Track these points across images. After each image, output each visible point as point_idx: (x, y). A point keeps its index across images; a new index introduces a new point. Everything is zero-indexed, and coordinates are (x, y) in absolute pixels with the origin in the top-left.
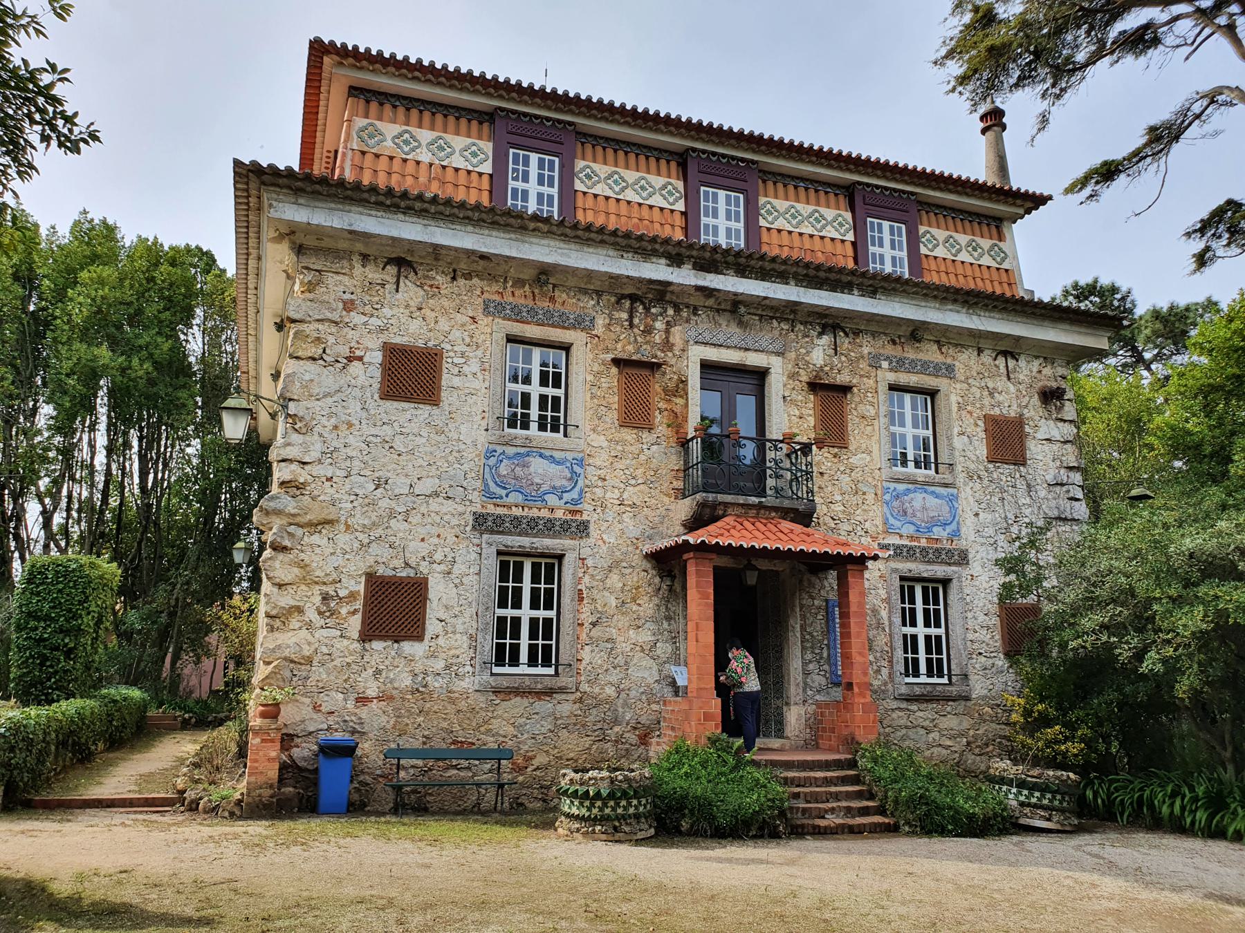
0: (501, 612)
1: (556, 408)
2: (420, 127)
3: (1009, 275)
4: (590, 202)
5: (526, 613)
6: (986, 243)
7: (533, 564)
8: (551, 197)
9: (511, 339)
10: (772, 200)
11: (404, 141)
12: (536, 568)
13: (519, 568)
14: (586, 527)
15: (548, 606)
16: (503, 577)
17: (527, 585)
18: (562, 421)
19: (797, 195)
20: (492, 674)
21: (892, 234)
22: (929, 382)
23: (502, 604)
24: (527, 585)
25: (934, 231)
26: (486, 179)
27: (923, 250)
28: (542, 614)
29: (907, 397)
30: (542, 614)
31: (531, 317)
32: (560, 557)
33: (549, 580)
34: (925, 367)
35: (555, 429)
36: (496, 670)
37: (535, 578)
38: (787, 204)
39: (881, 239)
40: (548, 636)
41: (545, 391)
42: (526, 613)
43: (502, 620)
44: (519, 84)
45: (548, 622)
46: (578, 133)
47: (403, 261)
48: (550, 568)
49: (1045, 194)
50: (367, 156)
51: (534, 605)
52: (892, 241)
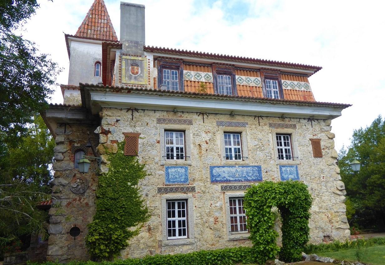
0: (232, 215)
1: (182, 151)
2: (251, 76)
3: (310, 94)
4: (189, 83)
5: (177, 219)
6: (303, 83)
7: (178, 203)
8: (277, 92)
9: (166, 130)
10: (293, 81)
11: (241, 80)
12: (179, 204)
13: (235, 201)
14: (194, 189)
15: (184, 216)
16: (169, 208)
17: (176, 210)
18: (184, 156)
19: (254, 74)
20: (167, 240)
21: (273, 84)
22: (238, 129)
23: (169, 216)
24: (176, 210)
25: (287, 81)
26: (211, 84)
27: (284, 88)
28: (182, 219)
29: (174, 134)
30: (182, 219)
31: (230, 124)
32: (187, 200)
33: (183, 207)
34: (180, 122)
35: (182, 158)
36: (169, 238)
37: (179, 207)
38: (291, 81)
39: (270, 86)
40: (184, 226)
41: (286, 147)
42: (177, 219)
43: (169, 222)
44: (194, 52)
45: (184, 221)
46: (236, 67)
47: (311, 119)
48: (183, 204)
49: (320, 66)
50: (188, 81)
51: (179, 216)
52: (274, 86)
